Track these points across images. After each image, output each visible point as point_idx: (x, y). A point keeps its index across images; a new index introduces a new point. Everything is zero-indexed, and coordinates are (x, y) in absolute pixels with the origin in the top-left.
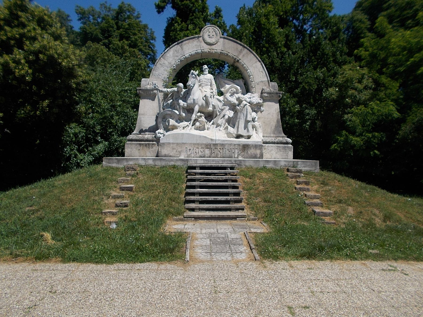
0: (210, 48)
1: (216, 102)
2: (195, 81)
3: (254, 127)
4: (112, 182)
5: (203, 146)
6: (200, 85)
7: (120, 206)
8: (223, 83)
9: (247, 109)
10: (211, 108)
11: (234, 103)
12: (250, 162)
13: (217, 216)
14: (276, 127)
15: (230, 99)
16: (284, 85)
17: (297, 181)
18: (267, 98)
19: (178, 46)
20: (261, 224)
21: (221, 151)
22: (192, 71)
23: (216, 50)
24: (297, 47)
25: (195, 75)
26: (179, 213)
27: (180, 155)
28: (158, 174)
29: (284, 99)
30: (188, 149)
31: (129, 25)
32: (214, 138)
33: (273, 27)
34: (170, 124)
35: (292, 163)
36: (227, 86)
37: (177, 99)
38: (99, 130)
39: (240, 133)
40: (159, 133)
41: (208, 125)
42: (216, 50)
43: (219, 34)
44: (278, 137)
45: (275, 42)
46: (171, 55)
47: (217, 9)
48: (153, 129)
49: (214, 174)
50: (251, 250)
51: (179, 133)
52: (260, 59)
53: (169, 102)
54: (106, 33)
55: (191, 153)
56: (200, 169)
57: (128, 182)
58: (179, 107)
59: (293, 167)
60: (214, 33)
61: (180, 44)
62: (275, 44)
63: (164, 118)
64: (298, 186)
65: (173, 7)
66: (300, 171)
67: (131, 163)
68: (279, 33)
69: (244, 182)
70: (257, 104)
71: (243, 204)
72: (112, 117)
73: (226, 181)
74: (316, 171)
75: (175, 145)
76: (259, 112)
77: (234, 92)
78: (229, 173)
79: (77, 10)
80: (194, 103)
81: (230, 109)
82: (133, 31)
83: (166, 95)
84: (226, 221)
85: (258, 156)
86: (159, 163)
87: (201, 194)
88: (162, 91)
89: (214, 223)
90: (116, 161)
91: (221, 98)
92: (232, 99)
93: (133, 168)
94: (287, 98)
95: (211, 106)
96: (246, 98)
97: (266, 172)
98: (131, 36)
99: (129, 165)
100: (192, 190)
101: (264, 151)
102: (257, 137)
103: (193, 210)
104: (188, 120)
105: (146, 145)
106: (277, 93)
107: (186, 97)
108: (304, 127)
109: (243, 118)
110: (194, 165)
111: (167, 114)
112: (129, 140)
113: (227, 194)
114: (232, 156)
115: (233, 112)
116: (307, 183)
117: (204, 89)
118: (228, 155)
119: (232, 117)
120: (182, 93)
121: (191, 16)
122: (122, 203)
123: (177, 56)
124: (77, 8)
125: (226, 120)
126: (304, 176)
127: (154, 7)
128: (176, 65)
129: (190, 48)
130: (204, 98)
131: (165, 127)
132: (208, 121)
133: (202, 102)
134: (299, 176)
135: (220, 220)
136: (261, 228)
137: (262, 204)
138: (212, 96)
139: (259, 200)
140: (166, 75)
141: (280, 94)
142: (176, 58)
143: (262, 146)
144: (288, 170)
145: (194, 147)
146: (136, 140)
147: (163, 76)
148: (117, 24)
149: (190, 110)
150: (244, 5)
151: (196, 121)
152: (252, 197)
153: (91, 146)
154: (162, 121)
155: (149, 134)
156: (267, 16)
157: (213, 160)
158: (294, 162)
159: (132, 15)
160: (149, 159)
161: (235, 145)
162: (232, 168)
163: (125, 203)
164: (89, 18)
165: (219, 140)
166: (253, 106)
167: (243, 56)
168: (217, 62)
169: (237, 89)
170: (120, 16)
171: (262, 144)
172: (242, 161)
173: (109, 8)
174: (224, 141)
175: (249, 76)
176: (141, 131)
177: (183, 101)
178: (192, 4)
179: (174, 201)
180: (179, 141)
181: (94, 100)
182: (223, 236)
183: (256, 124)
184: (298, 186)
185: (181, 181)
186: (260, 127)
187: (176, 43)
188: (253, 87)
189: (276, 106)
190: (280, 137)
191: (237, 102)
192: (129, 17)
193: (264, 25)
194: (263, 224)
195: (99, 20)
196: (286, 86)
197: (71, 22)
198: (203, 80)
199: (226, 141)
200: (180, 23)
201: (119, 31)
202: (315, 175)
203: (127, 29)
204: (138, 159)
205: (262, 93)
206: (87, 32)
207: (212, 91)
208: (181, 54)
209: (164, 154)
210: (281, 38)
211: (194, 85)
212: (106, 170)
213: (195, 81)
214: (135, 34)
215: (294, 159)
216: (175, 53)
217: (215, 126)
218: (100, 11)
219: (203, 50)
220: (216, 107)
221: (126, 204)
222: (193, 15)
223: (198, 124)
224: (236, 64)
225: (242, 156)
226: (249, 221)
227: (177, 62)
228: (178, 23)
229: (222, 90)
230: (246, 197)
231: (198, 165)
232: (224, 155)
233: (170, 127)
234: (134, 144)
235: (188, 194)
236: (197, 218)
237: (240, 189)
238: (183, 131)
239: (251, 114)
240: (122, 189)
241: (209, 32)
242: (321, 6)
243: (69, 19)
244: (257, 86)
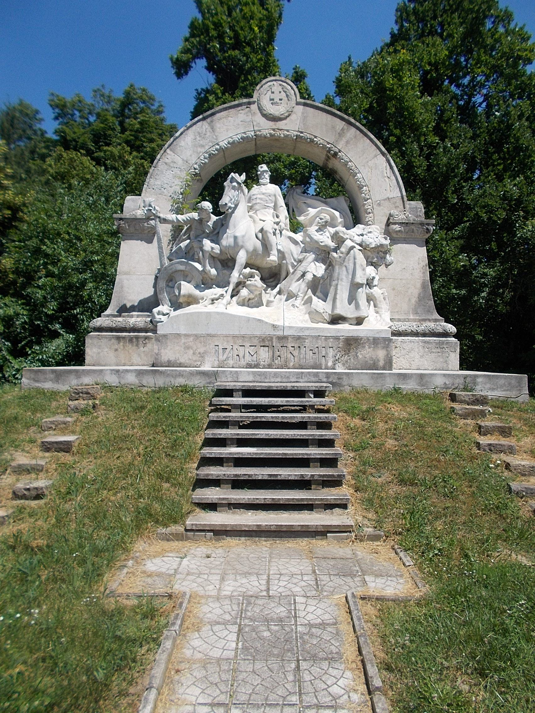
0: (274, 127)
1: (284, 244)
2: (238, 196)
3: (370, 298)
4: (28, 428)
5: (256, 342)
6: (251, 208)
7: (24, 497)
8: (304, 206)
9: (355, 259)
10: (274, 258)
11: (326, 246)
12: (362, 379)
13: (273, 528)
14: (421, 299)
15: (317, 236)
16: (435, 212)
17: (480, 427)
18: (400, 235)
19: (204, 122)
20: (393, 554)
21: (296, 353)
22: (232, 174)
23: (288, 131)
24: (460, 135)
25: (238, 183)
26: (175, 517)
27: (202, 363)
28: (143, 408)
29: (434, 241)
30: (221, 347)
31: (141, 123)
32: (280, 323)
33: (411, 92)
34: (182, 292)
35: (462, 381)
36: (312, 211)
37: (199, 238)
38: (53, 310)
40: (159, 313)
41: (270, 295)
42: (288, 131)
43: (294, 97)
44: (425, 320)
45: (415, 123)
46: (190, 144)
47: (296, 72)
48: (147, 306)
49: (277, 409)
50: (370, 693)
51: (201, 313)
52: (383, 149)
53: (183, 245)
54: (101, 138)
55: (228, 358)
56: (244, 396)
57: (64, 428)
58: (203, 255)
59: (465, 389)
60: (283, 94)
61: (209, 120)
62: (415, 128)
63: (171, 280)
64: (484, 440)
65: (209, 68)
66: (482, 401)
67: (87, 380)
68: (424, 104)
69: (348, 427)
70: (377, 247)
71: (344, 492)
72: (83, 284)
73: (302, 425)
74: (520, 399)
75: (191, 339)
76: (383, 266)
77: (326, 222)
78: (312, 407)
79: (52, 100)
80: (237, 245)
81: (316, 260)
82: (149, 136)
83: (177, 229)
84: (299, 540)
85: (381, 363)
86: (150, 382)
87: (240, 462)
88: (165, 221)
89: (264, 546)
90: (52, 376)
91: (299, 237)
92: (321, 237)
93: (87, 393)
94: (442, 239)
95: (275, 252)
96: (353, 234)
97: (400, 402)
98: (145, 144)
99: (81, 385)
100: (216, 451)
101: (394, 353)
102: (378, 322)
103: (212, 507)
104: (223, 284)
105: (131, 340)
106: (422, 224)
107: (218, 233)
108: (475, 301)
109: (347, 277)
110: (230, 385)
111: (176, 271)
112: (100, 329)
113: (304, 462)
114: (321, 364)
115: (324, 267)
116: (505, 432)
117: (260, 215)
118: (311, 362)
119: (322, 277)
120: (210, 224)
121: (243, 82)
122: (28, 490)
123: (202, 146)
124: (52, 98)
126: (494, 414)
127: (170, 64)
128: (200, 166)
129: (232, 126)
130: (260, 235)
131: (174, 299)
132: (268, 286)
133: (254, 243)
134: (483, 414)
135: (281, 537)
136: (395, 578)
137: (394, 489)
138: (278, 232)
139: (386, 476)
140: (178, 188)
141: (428, 224)
142: (199, 150)
143: (390, 340)
144: (453, 398)
145: (235, 343)
146: (111, 330)
147: (172, 190)
148: (121, 123)
149: (226, 262)
150: (350, 58)
151: (240, 287)
152: (370, 470)
153: (39, 343)
154: (168, 286)
155: (138, 316)
156: (397, 72)
157: (276, 375)
158: (465, 377)
159: (150, 108)
160: (127, 371)
161: (327, 338)
162: (319, 394)
163: (36, 488)
164: (73, 115)
166: (369, 253)
167: (347, 142)
168: (293, 171)
169: (333, 218)
170: (127, 111)
171: (389, 335)
172: (345, 377)
173: (109, 97)
174: (302, 329)
175: (360, 187)
176: (123, 310)
177: (212, 241)
178: (243, 56)
179: (167, 481)
180: (201, 330)
181: (49, 251)
182: (281, 611)
183: (376, 291)
184: (484, 440)
185: (195, 425)
186: (384, 299)
187: (201, 117)
188: (369, 211)
189: (422, 253)
190: (429, 320)
191: (332, 245)
192: (142, 111)
193: (391, 90)
194: (402, 554)
195: (92, 119)
196: (439, 215)
197: (42, 122)
198: (259, 196)
199: (308, 329)
200: (220, 95)
201: (124, 136)
202: (520, 410)
203: (137, 131)
204: (101, 371)
205: (388, 224)
206: (68, 138)
207: (277, 220)
208: (210, 141)
209: (166, 359)
210: (426, 116)
211: (236, 206)
212: (25, 399)
213: (238, 196)
214: (152, 141)
215: (461, 368)
216: (198, 138)
217: (284, 297)
218: (93, 103)
219: (260, 131)
220: (286, 255)
221: (39, 492)
222: (246, 79)
223: (244, 292)
224: (334, 164)
225: (344, 364)
226: (361, 541)
227: (202, 158)
228: (216, 94)
229: (301, 219)
230: (352, 469)
231: (239, 385)
232: (303, 362)
233: (181, 300)
234: (105, 337)
235: (206, 461)
236: (220, 533)
237: (338, 449)
238: (211, 308)
239: (364, 270)
240: (47, 447)
241: (273, 93)
242: (511, 49)
243: (38, 116)
244: (377, 210)
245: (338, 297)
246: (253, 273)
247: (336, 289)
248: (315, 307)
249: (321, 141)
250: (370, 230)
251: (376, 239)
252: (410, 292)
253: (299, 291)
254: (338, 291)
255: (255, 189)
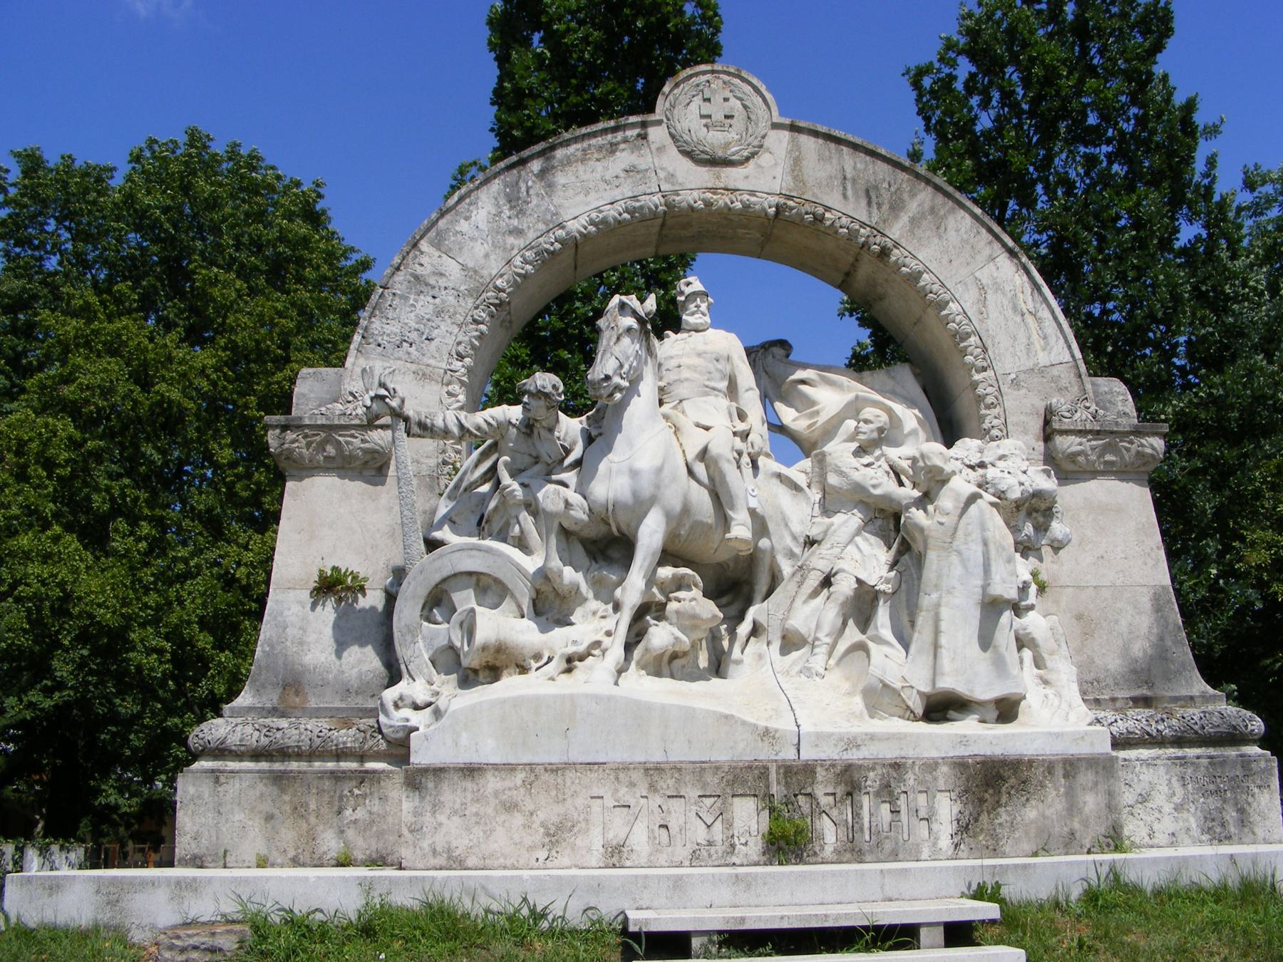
23: (752, 193)
39: (950, 682)
75: (520, 777)
123: (518, 232)
125: (843, 605)
129: (594, 184)
130: (700, 469)
138: (746, 459)
142: (511, 240)
143: (1113, 760)
165: (820, 737)
171: (1106, 747)
174: (852, 743)
183: (1034, 622)
198: (685, 361)
207: (741, 427)
219: (676, 193)
223: (661, 635)
227: (518, 261)
244: (1012, 400)
245: (943, 640)
246: (683, 576)
247: (937, 620)
248: (878, 673)
249: (844, 220)
250: (1001, 452)
251: (1023, 478)
252: (1124, 623)
253: (818, 627)
254: (943, 626)
255: (672, 345)
